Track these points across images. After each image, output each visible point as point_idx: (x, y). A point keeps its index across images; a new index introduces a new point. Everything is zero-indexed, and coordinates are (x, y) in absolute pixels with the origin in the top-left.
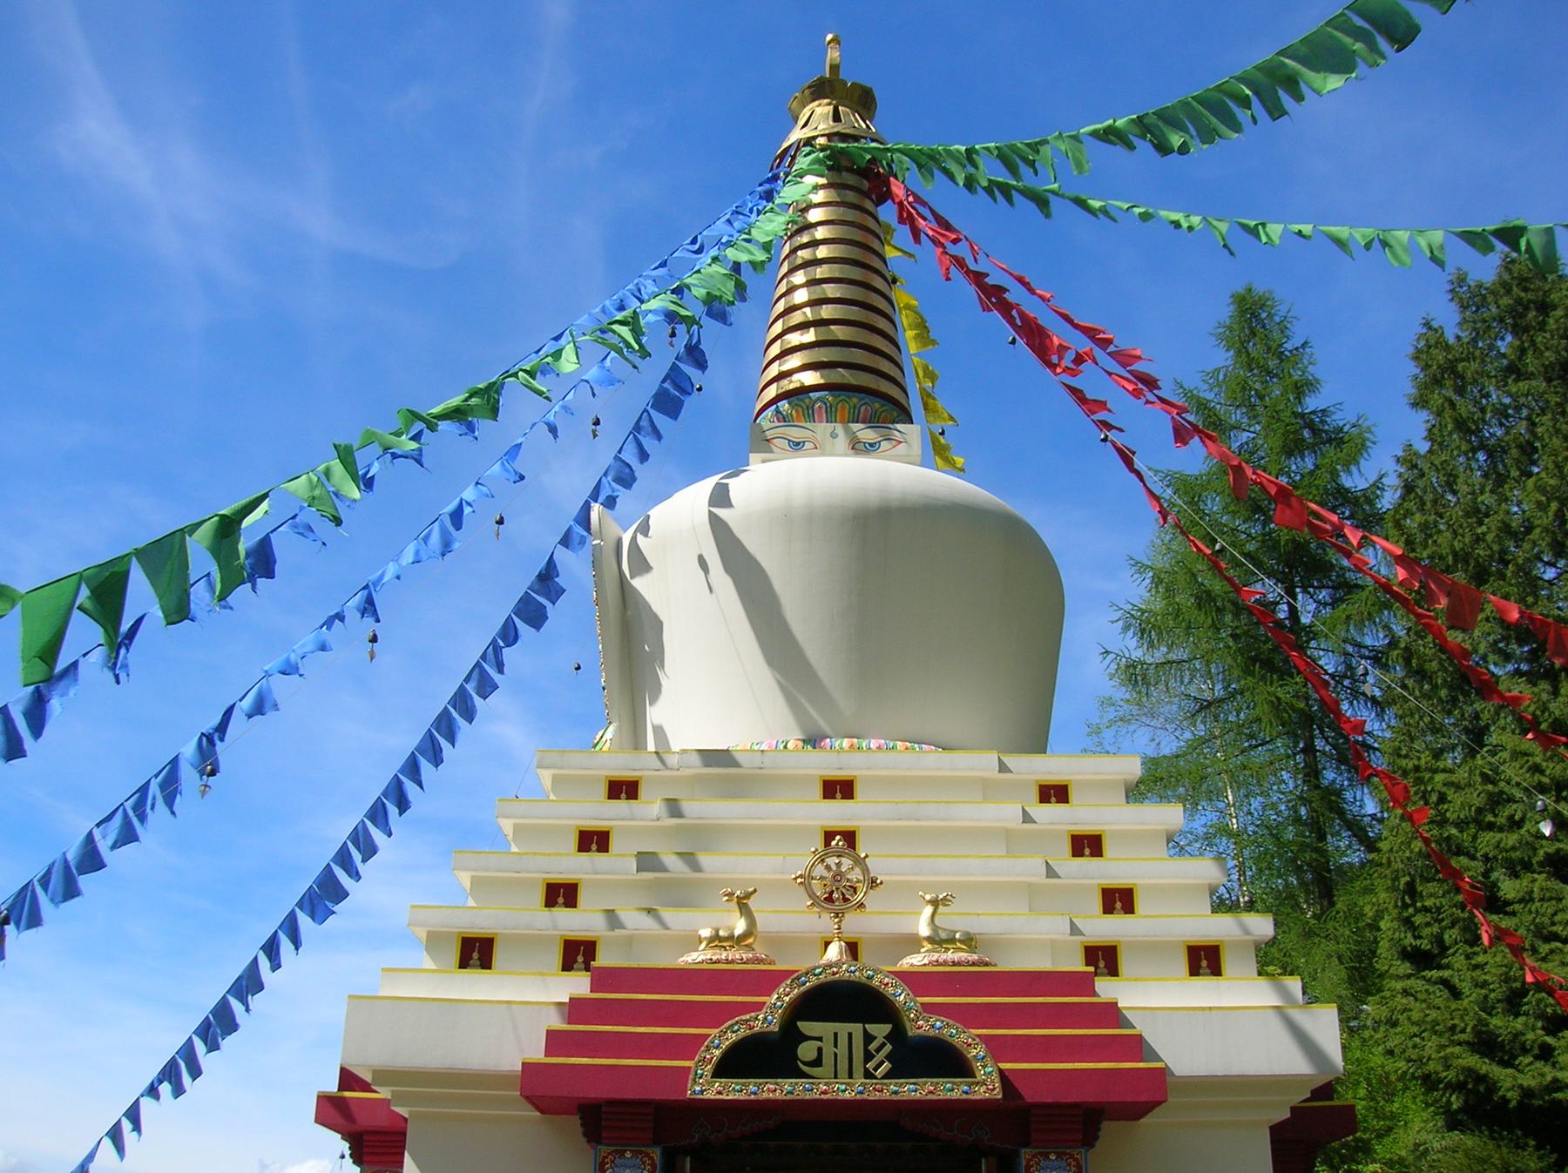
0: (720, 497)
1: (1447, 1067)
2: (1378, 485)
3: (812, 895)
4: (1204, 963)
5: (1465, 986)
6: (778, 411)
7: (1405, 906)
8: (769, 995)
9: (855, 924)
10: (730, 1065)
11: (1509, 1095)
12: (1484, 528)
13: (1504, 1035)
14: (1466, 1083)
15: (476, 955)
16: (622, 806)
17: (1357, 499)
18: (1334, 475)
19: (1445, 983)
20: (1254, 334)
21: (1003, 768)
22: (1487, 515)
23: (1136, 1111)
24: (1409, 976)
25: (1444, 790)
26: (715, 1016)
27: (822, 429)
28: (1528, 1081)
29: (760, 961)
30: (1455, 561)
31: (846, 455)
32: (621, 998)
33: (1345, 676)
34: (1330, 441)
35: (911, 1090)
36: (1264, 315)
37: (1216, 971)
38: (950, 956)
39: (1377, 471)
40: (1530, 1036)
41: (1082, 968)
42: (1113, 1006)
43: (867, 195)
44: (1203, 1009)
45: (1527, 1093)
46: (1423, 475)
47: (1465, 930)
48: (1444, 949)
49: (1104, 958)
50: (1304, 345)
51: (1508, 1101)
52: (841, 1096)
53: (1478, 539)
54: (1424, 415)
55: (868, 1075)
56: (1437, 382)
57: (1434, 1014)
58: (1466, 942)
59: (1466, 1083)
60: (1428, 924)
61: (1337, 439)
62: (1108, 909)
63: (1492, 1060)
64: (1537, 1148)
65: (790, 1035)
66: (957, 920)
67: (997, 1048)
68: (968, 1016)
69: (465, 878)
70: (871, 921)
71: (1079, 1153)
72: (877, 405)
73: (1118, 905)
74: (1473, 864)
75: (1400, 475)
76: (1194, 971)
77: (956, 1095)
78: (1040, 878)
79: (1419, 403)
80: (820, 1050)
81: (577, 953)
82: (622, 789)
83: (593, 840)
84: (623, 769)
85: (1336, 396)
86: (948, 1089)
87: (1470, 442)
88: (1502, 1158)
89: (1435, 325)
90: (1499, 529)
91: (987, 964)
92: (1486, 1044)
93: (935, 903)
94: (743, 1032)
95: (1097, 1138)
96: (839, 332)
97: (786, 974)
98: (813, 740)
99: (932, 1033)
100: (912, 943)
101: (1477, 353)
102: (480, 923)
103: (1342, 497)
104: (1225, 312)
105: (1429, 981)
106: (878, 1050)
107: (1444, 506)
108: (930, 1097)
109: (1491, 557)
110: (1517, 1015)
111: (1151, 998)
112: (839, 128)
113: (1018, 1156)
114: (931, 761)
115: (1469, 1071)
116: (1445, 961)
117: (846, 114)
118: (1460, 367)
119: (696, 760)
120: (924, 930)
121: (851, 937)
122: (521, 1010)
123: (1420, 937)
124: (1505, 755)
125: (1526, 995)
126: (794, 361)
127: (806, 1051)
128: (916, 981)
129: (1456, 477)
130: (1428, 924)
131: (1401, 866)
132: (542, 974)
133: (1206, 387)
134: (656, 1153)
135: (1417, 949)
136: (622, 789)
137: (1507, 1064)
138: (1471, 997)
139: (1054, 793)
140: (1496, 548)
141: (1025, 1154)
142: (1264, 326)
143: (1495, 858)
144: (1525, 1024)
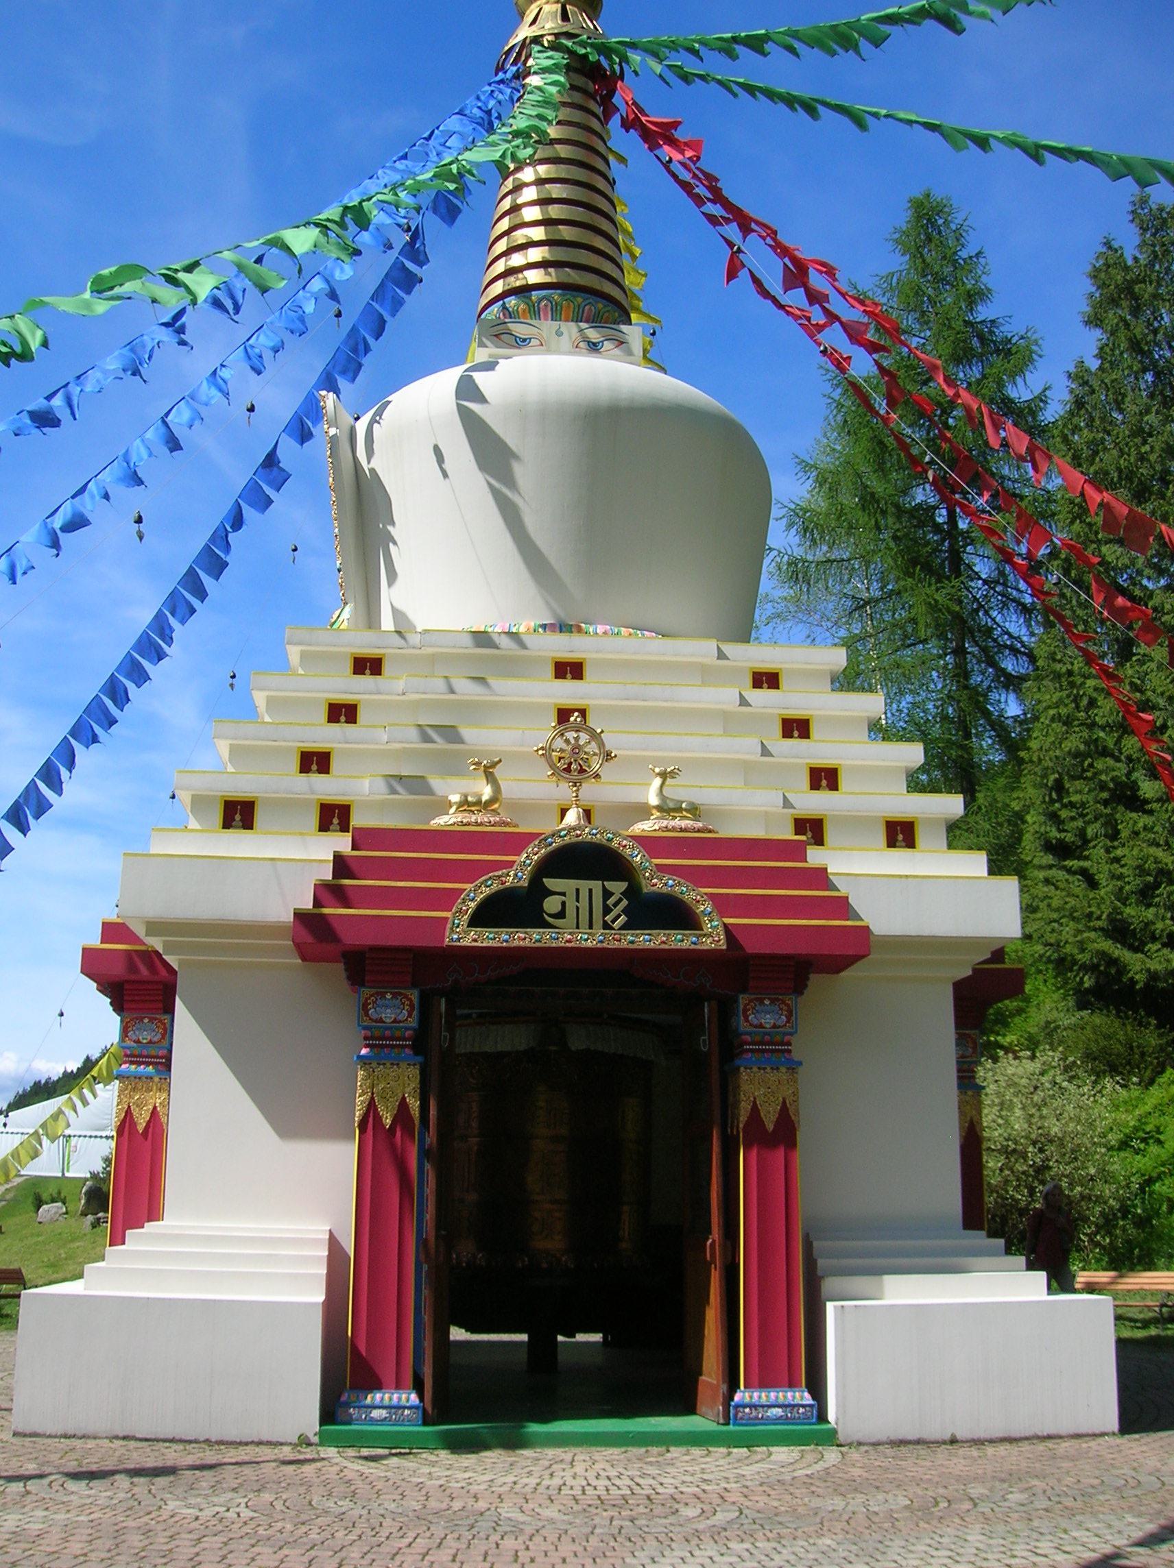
0: (467, 390)
1: (1083, 950)
2: (1042, 399)
3: (552, 766)
4: (900, 837)
5: (1102, 878)
6: (504, 307)
7: (1052, 801)
8: (519, 854)
9: (591, 792)
10: (482, 918)
11: (1137, 977)
12: (1147, 448)
13: (1136, 924)
14: (1098, 965)
15: (238, 817)
16: (367, 681)
17: (1021, 410)
18: (1000, 385)
19: (1084, 872)
20: (929, 239)
21: (721, 655)
22: (1151, 435)
23: (838, 965)
24: (1050, 867)
25: (1095, 695)
26: (471, 872)
27: (547, 327)
28: (1154, 966)
29: (506, 824)
30: (1120, 478)
31: (570, 353)
32: (371, 858)
33: (997, 582)
34: (998, 351)
35: (645, 940)
36: (940, 222)
37: (910, 844)
38: (677, 823)
39: (1048, 384)
40: (1160, 925)
41: (791, 836)
42: (823, 871)
43: (592, 96)
44: (900, 876)
45: (1153, 976)
46: (1093, 392)
47: (1105, 825)
48: (1086, 841)
49: (812, 829)
50: (978, 255)
51: (1137, 982)
52: (584, 945)
53: (1142, 458)
54: (1097, 333)
55: (606, 926)
56: (1114, 302)
57: (1072, 902)
58: (1106, 836)
59: (1098, 965)
60: (1073, 819)
61: (1005, 349)
62: (815, 785)
63: (1124, 944)
64: (1158, 1027)
65: (536, 890)
66: (680, 791)
67: (723, 905)
68: (698, 877)
69: (223, 747)
70: (608, 789)
71: (790, 999)
72: (600, 306)
73: (824, 783)
74: (1118, 765)
75: (1071, 391)
76: (891, 843)
77: (685, 945)
78: (756, 756)
79: (1094, 321)
80: (563, 904)
81: (333, 816)
82: (368, 665)
83: (342, 713)
84: (366, 646)
85: (1004, 310)
86: (678, 940)
87: (1141, 362)
88: (1126, 1034)
89: (1115, 245)
90: (1163, 450)
91: (710, 831)
92: (1120, 931)
93: (664, 775)
94: (496, 887)
95: (806, 986)
96: (566, 232)
97: (532, 837)
98: (562, 627)
99: (665, 890)
100: (643, 811)
101: (1154, 276)
102: (242, 788)
103: (1008, 407)
104: (903, 218)
105: (1069, 871)
106: (616, 905)
107: (1111, 423)
108: (663, 946)
109: (1153, 476)
110: (1149, 906)
111: (857, 867)
112: (568, 28)
113: (736, 1001)
114: (654, 647)
115: (1103, 954)
116: (1086, 853)
117: (574, 14)
118: (1137, 288)
119: (468, 641)
120: (654, 800)
121: (587, 804)
122: (284, 868)
123: (1066, 831)
124: (1153, 665)
125: (1158, 887)
126: (517, 260)
127: (551, 905)
128: (649, 844)
129: (1124, 395)
130: (1073, 819)
131: (1051, 764)
132: (301, 834)
133: (879, 292)
134: (414, 995)
135: (1061, 842)
136: (368, 665)
137: (1136, 950)
138: (1107, 888)
139: (767, 679)
140: (1158, 468)
141: (743, 999)
142: (940, 233)
143: (1138, 760)
144: (1156, 915)
